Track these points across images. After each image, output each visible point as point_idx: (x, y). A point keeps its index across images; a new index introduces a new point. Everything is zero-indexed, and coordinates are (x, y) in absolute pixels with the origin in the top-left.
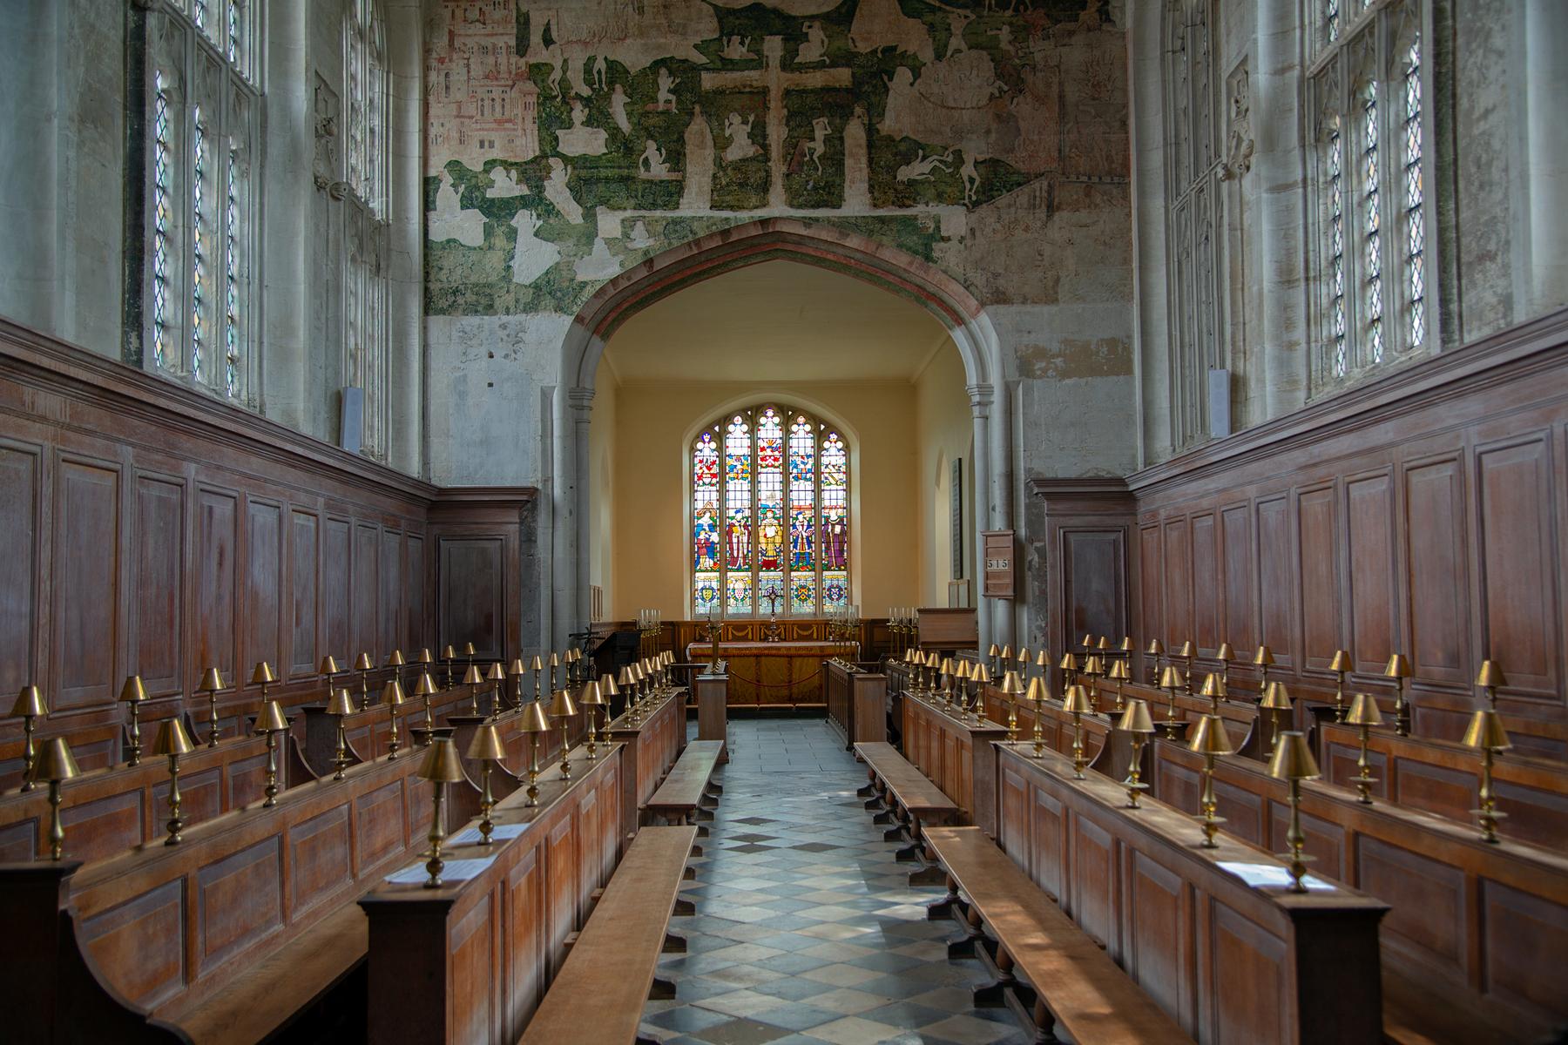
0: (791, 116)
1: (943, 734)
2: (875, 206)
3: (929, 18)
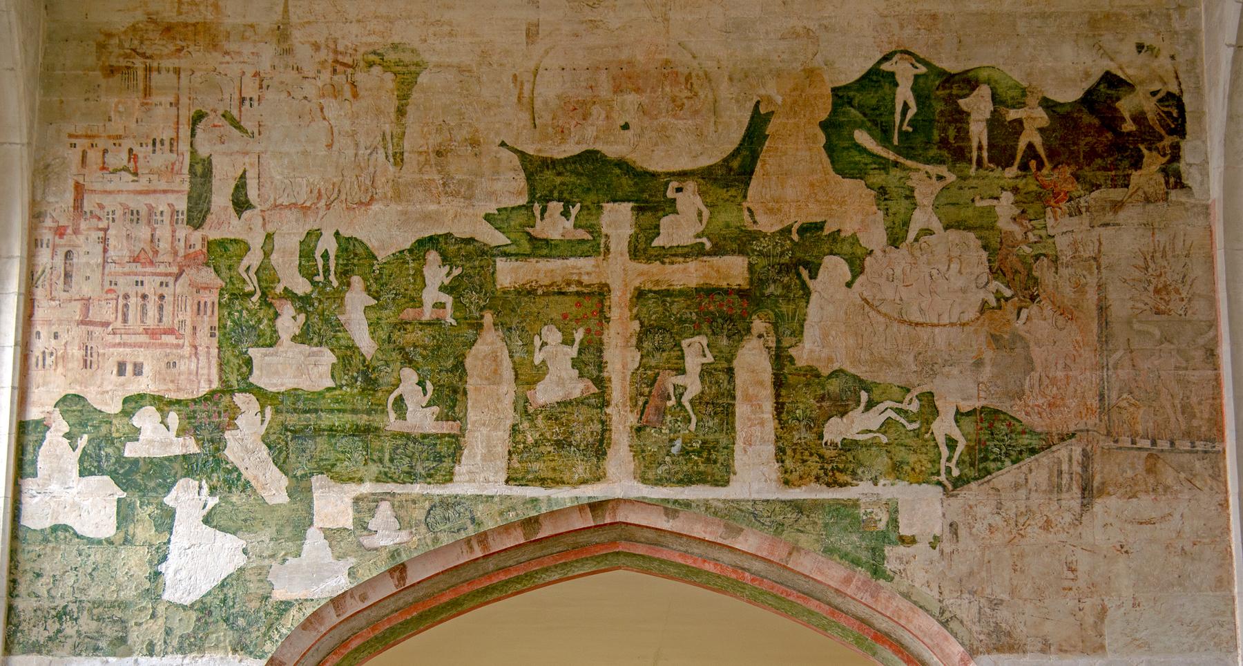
2: (786, 482)
3: (878, 178)
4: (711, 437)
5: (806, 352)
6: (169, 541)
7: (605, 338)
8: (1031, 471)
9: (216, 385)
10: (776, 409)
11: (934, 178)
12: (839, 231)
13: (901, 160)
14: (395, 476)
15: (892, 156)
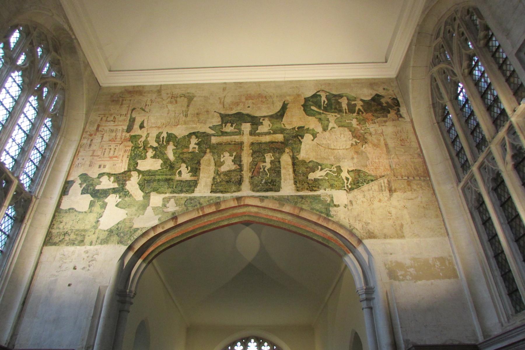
2: (298, 190)
3: (319, 116)
4: (274, 179)
5: (302, 155)
6: (104, 212)
7: (242, 154)
8: (373, 186)
9: (126, 169)
10: (293, 171)
11: (334, 116)
12: (309, 128)
13: (324, 112)
14: (177, 192)
15: (322, 112)
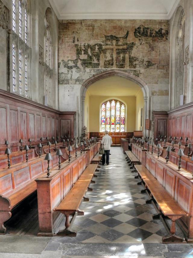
0: (117, 53)
1: (137, 150)
3: (139, 38)
